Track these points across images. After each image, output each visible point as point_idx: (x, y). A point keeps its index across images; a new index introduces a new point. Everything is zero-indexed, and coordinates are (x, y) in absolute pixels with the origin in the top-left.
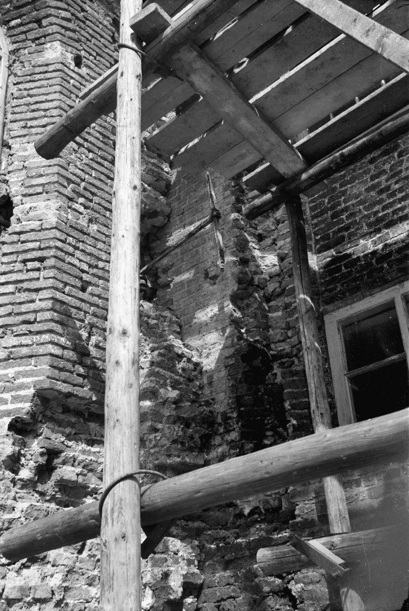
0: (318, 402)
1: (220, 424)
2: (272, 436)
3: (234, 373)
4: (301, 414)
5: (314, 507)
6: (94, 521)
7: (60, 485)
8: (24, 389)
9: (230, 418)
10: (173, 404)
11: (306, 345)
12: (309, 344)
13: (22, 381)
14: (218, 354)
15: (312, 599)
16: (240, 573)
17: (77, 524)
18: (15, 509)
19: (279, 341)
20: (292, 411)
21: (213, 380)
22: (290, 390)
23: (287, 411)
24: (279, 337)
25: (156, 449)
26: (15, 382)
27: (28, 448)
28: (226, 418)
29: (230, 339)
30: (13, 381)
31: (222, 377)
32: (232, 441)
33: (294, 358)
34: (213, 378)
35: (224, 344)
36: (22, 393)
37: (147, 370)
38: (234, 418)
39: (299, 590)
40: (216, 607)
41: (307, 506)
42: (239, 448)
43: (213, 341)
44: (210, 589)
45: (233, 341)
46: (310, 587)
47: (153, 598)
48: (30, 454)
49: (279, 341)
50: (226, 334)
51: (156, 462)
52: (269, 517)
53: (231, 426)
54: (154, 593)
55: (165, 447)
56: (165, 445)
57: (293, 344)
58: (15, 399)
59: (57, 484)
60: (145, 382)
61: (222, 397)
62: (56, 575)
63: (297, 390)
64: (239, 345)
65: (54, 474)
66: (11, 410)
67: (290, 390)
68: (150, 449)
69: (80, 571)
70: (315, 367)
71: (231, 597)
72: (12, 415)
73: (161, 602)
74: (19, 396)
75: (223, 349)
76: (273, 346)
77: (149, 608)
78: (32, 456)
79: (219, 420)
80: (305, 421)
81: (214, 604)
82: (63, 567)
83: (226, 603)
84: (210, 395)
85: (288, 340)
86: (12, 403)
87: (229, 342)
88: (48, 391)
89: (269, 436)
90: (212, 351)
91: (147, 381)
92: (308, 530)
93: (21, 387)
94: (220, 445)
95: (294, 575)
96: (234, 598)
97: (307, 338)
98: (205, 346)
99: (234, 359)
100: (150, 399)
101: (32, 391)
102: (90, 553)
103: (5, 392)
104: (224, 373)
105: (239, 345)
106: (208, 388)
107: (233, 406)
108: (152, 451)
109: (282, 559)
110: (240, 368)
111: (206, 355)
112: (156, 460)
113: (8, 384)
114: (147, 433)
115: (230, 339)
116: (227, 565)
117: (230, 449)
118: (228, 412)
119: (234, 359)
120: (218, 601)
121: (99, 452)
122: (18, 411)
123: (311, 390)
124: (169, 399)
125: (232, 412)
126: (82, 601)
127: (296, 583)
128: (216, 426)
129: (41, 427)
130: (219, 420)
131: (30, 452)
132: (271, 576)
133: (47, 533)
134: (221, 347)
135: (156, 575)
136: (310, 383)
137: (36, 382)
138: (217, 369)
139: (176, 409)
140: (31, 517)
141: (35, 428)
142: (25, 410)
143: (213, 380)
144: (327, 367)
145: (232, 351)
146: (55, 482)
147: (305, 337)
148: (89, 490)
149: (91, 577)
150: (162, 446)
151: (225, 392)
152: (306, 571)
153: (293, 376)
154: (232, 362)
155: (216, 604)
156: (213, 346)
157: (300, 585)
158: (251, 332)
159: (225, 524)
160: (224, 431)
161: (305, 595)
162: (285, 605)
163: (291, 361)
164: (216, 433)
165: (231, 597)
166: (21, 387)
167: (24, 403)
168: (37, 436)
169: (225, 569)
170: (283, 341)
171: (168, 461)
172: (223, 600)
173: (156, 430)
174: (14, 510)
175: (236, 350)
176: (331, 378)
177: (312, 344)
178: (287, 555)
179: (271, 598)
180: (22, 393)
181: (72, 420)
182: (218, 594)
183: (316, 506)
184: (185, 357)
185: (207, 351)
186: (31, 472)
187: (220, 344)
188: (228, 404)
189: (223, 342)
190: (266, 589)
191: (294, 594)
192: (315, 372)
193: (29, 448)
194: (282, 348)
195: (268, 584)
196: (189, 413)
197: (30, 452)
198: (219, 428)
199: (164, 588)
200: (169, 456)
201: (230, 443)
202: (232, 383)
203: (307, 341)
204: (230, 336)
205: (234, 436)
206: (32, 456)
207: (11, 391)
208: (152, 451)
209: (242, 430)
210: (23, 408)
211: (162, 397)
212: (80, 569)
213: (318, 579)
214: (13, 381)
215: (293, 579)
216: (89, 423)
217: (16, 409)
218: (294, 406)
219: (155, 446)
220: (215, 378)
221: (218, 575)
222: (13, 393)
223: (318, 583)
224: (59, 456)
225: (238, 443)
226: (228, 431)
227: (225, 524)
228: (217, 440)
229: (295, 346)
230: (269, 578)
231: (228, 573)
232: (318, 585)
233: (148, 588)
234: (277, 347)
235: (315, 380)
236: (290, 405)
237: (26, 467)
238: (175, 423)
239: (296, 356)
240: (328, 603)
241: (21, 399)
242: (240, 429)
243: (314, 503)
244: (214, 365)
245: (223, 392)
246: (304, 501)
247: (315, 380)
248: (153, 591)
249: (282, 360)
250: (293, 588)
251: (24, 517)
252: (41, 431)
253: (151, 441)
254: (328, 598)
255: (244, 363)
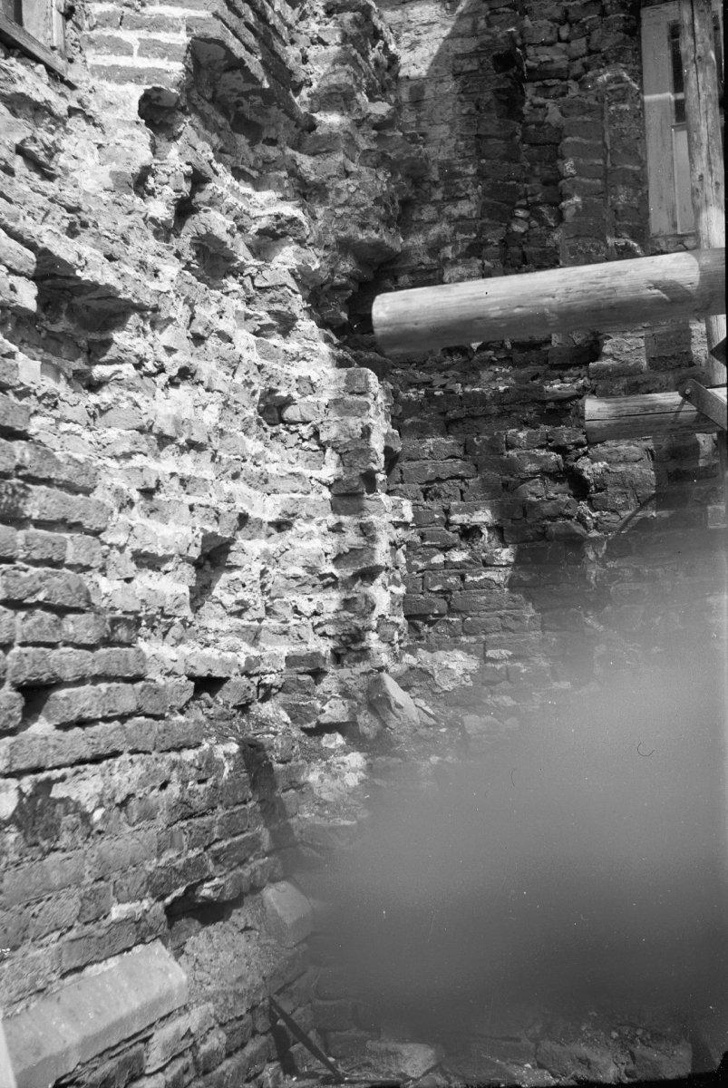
0: (712, 161)
1: (435, 184)
2: (527, 220)
3: (475, 89)
4: (590, 186)
5: (642, 343)
6: (656, 291)
7: (200, 245)
8: (167, 31)
9: (459, 175)
10: (373, 129)
11: (695, 52)
12: (702, 51)
13: (161, 12)
14: (437, 47)
15: (623, 485)
16: (477, 440)
17: (610, 294)
18: (160, 274)
19: (543, 44)
20: (577, 178)
21: (425, 97)
22: (577, 139)
23: (565, 178)
24: (544, 36)
25: (347, 210)
26: (143, 10)
27: (159, 158)
28: (449, 175)
29: (470, 20)
30: (139, 7)
31: (447, 94)
32: (462, 217)
33: (570, 82)
34: (423, 93)
35: (453, 28)
36: (163, 37)
37: (337, 48)
38: (469, 175)
39: (599, 471)
40: (422, 490)
41: (629, 341)
42: (475, 231)
43: (426, 18)
44: (410, 463)
45: (475, 24)
46: (621, 468)
47: (338, 466)
48: (164, 172)
49: (543, 44)
50: (460, 9)
51: (342, 234)
52: (518, 356)
53: (461, 190)
54: (341, 459)
55: (362, 209)
56: (363, 205)
57: (575, 54)
58: (148, 48)
59: (195, 241)
60: (334, 73)
61: (444, 132)
62: (210, 407)
63: (588, 141)
64: (489, 34)
65: (189, 221)
66: (143, 70)
67: (577, 139)
68: (336, 207)
69: (234, 406)
70: (710, 96)
71: (457, 477)
72: (145, 81)
73: (356, 473)
74: (156, 43)
75: (450, 37)
76: (530, 51)
77: (332, 482)
78: (169, 175)
79: (435, 176)
80: (596, 200)
81: (419, 487)
82: (219, 394)
83: (444, 485)
84: (414, 125)
85: (559, 45)
86: (140, 54)
87: (466, 25)
88: (212, 46)
89: (522, 218)
90: (424, 37)
91: (340, 71)
92: (625, 380)
93: (159, 24)
94: (433, 222)
95: (589, 449)
96: (462, 478)
97: (698, 38)
98: (408, 26)
99: (475, 62)
100: (341, 111)
101: (182, 39)
102: (246, 377)
103: (125, 28)
104: (450, 86)
105: (489, 34)
106: (410, 110)
107: (468, 153)
108: (339, 212)
109: (638, 417)
110: (489, 81)
111: (408, 43)
112: (342, 230)
113: (127, 11)
114: (335, 176)
115: (470, 20)
116: (448, 427)
117: (455, 231)
118: (455, 162)
119: (475, 62)
120: (427, 483)
121: (250, 196)
122: (159, 76)
123: (699, 138)
124: (372, 117)
125: (465, 165)
126: (239, 457)
127: (594, 460)
128: (426, 186)
129: (181, 122)
130: (435, 176)
131: (164, 168)
132: (541, 447)
133: (519, 307)
134: (445, 33)
135: (353, 430)
136: (699, 125)
137: (190, 19)
138: (434, 76)
139: (376, 139)
140: (183, 295)
141: (169, 121)
142: (173, 76)
143: (425, 97)
144: (638, 107)
145: (471, 45)
146: (192, 238)
147: (694, 35)
148: (236, 265)
149: (248, 420)
150: (357, 206)
151: (452, 125)
152: (614, 444)
153: (584, 114)
154: (469, 68)
155: (424, 486)
156: (426, 28)
157: (601, 465)
158: (498, 14)
159: (422, 361)
160: (444, 198)
161: (609, 479)
162: (564, 493)
163: (563, 86)
164: (426, 200)
165: (457, 477)
166: (159, 24)
167: (170, 59)
168: (175, 138)
169: (446, 432)
170: (550, 44)
171: (361, 236)
172: (439, 480)
173: (348, 174)
174: (156, 276)
175: (482, 45)
176: (644, 128)
177: (707, 52)
178: (651, 412)
179: (537, 482)
180: (163, 37)
181: (219, 121)
182: (430, 471)
183: (646, 343)
184: (382, 39)
185: (412, 35)
186: (168, 208)
187: (444, 26)
188: (456, 149)
189: (452, 23)
190: (531, 467)
191: (588, 477)
192: (710, 105)
193: (163, 160)
194: (547, 58)
195: (535, 459)
196: (400, 151)
197: (164, 168)
198: (433, 190)
199: (362, 451)
200: (363, 226)
201: (457, 220)
202: (468, 108)
203: (699, 45)
204: (469, 15)
205: (464, 208)
206: (169, 175)
207: (139, 28)
208: (339, 212)
209: (483, 200)
210: (167, 72)
211: (360, 110)
212: (236, 402)
213: (638, 457)
214: (139, 7)
215: (585, 454)
216: (237, 135)
217: (154, 69)
218: (580, 170)
219: (346, 203)
220: (429, 93)
221: (430, 441)
222: (143, 34)
223: (636, 461)
224: (201, 187)
225: (473, 223)
226: (454, 199)
227: (422, 361)
228: (428, 213)
229: (576, 59)
230: (537, 450)
231: (450, 441)
232: (637, 466)
233: (329, 450)
234: (537, 55)
235: (710, 121)
236: (576, 167)
237: (159, 197)
238: (378, 167)
239: (576, 78)
240: (654, 492)
241: (165, 51)
242: (480, 198)
243: (642, 337)
244: (427, 66)
245: (447, 123)
246: (624, 332)
247: (710, 121)
248: (341, 454)
249: (547, 81)
250: (586, 468)
251: (175, 291)
252: (181, 129)
253: (339, 192)
254: (654, 484)
255: (498, 72)
